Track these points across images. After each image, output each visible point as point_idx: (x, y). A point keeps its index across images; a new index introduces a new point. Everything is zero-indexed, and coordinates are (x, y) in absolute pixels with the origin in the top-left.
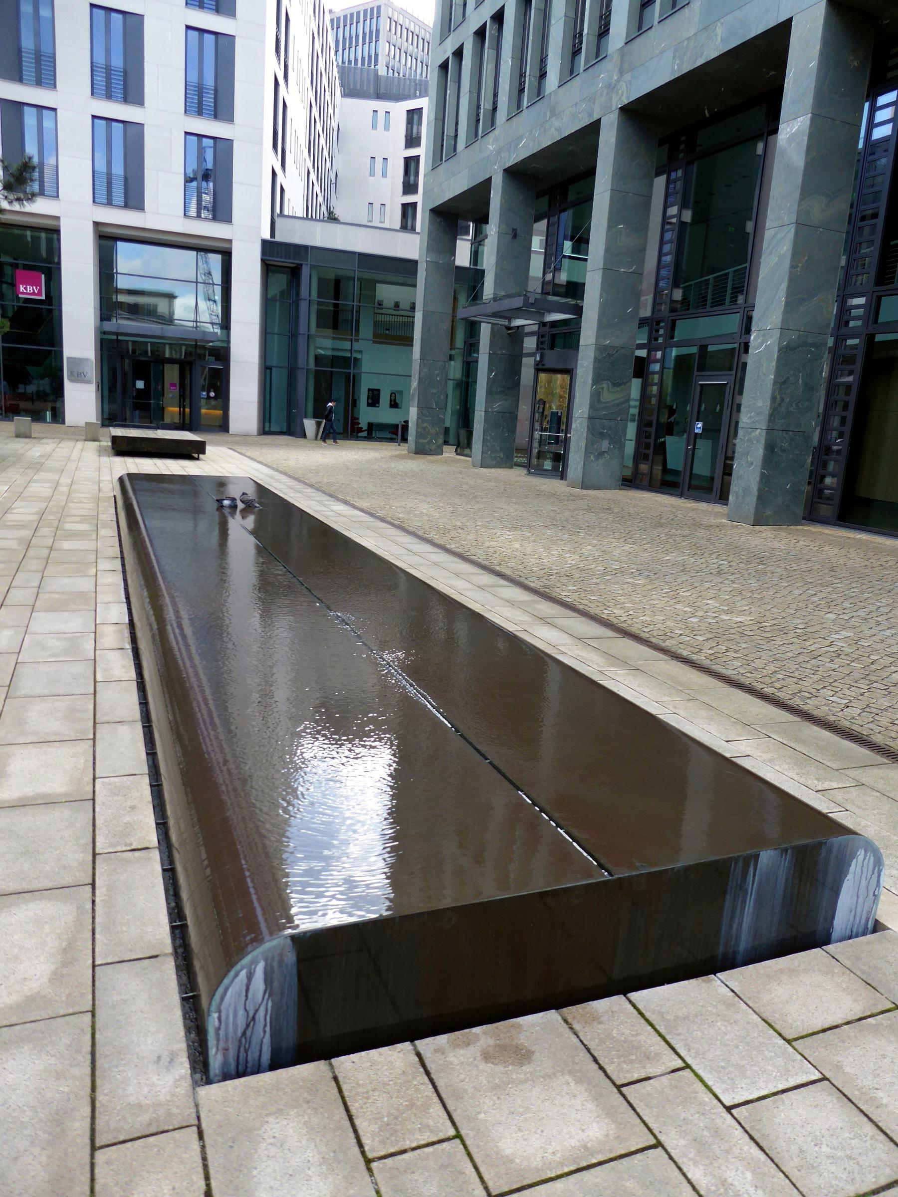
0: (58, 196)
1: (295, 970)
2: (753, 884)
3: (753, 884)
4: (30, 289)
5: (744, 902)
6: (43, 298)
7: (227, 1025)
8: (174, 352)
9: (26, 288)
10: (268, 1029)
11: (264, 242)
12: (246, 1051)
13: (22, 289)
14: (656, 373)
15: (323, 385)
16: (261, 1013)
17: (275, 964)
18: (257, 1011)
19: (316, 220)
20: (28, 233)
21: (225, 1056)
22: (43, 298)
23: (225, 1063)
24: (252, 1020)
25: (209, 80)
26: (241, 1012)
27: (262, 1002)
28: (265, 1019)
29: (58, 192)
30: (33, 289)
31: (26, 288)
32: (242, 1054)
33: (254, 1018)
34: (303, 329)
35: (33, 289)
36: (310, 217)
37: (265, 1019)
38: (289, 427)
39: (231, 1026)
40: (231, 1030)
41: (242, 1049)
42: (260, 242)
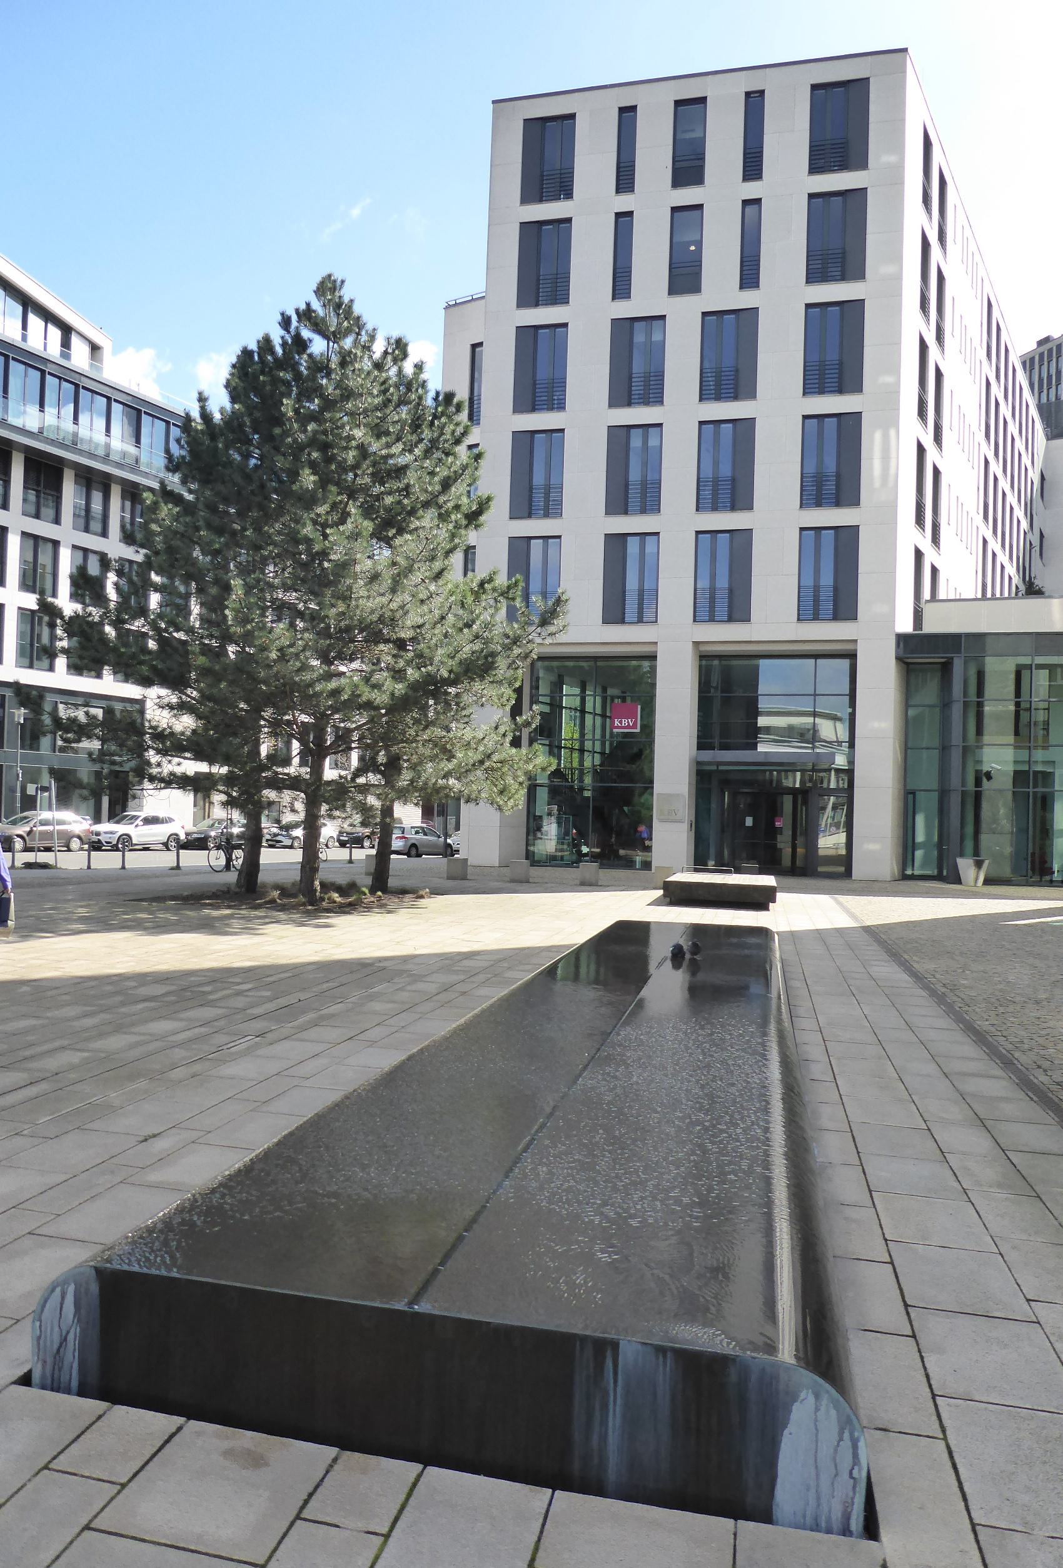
0: (656, 622)
1: (97, 1302)
2: (616, 1381)
3: (616, 1381)
4: (625, 722)
5: (605, 1407)
6: (638, 730)
7: (46, 1337)
8: (841, 782)
9: (621, 722)
10: (77, 1354)
11: (902, 639)
12: (60, 1370)
13: (617, 723)
14: (597, 740)
15: (1002, 811)
16: (71, 1337)
17: (83, 1290)
18: (68, 1332)
19: (1002, 598)
20: (716, 662)
21: (44, 1367)
22: (638, 730)
23: (43, 1376)
24: (63, 1340)
25: (831, 466)
26: (56, 1329)
27: (72, 1325)
28: (75, 1344)
29: (657, 617)
30: (628, 722)
31: (621, 722)
32: (56, 1371)
33: (65, 1339)
34: (956, 738)
35: (628, 722)
36: (989, 595)
37: (75, 1344)
38: (940, 869)
39: (48, 1339)
40: (48, 1343)
41: (56, 1367)
42: (894, 638)
